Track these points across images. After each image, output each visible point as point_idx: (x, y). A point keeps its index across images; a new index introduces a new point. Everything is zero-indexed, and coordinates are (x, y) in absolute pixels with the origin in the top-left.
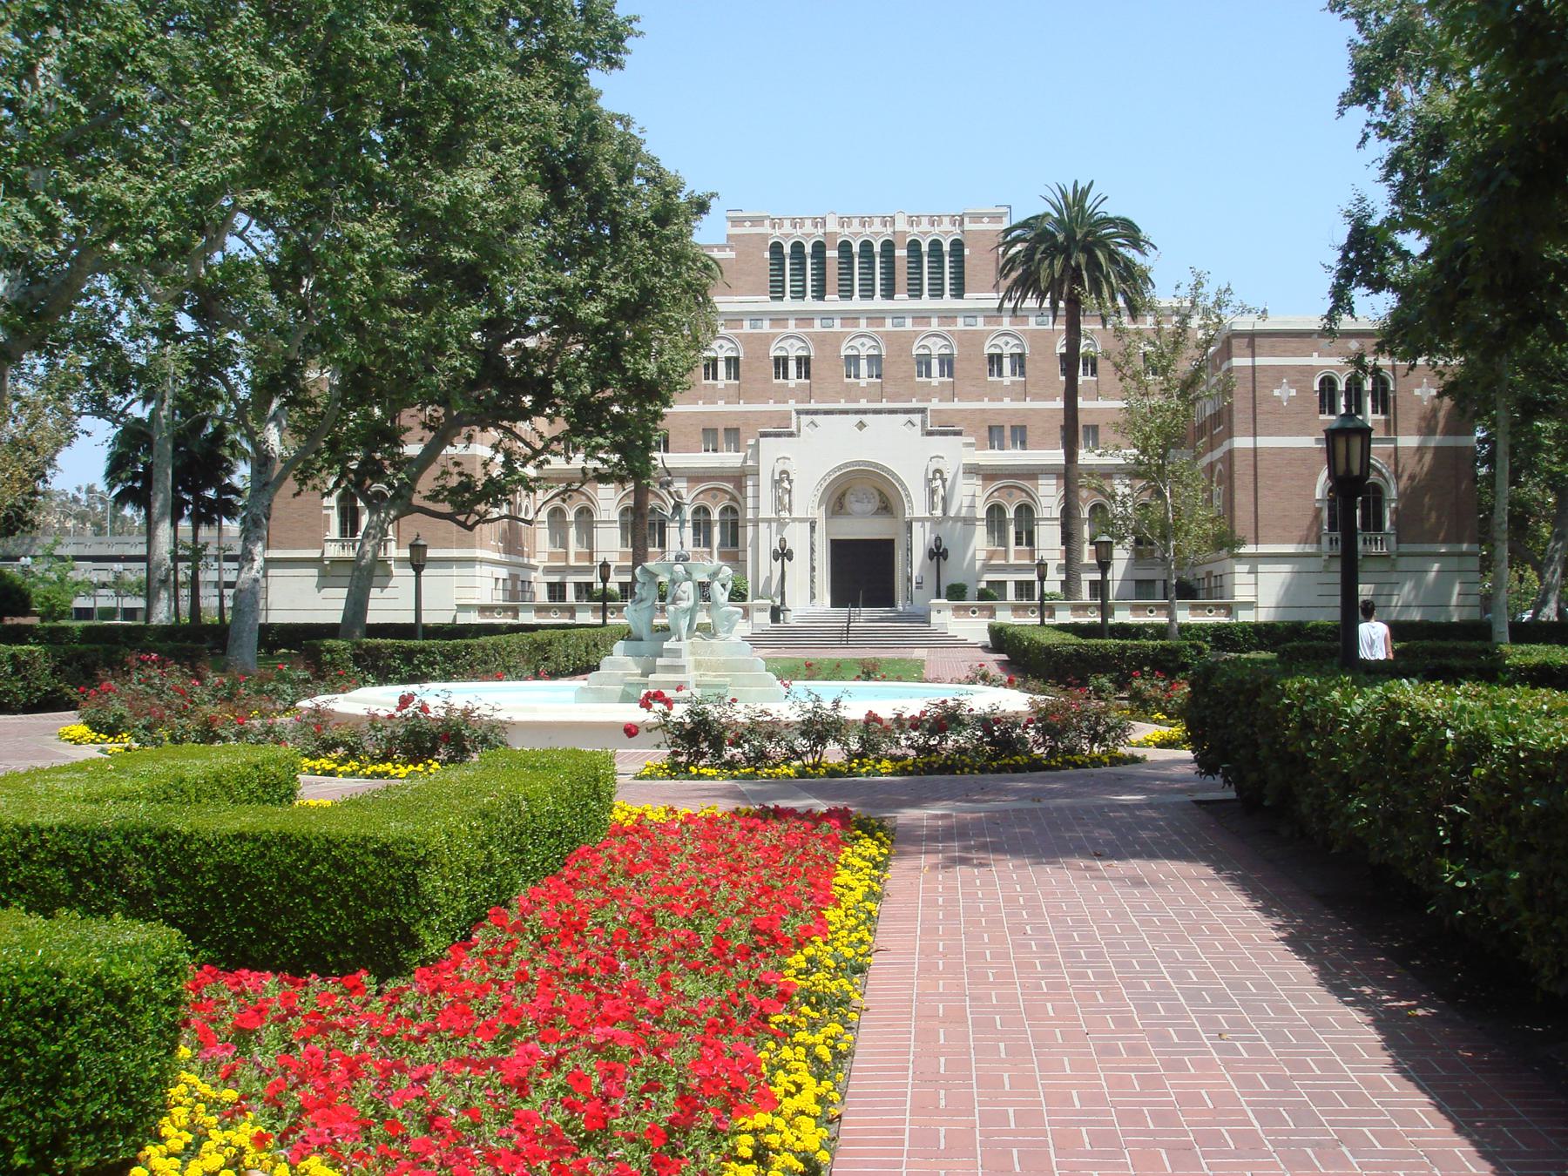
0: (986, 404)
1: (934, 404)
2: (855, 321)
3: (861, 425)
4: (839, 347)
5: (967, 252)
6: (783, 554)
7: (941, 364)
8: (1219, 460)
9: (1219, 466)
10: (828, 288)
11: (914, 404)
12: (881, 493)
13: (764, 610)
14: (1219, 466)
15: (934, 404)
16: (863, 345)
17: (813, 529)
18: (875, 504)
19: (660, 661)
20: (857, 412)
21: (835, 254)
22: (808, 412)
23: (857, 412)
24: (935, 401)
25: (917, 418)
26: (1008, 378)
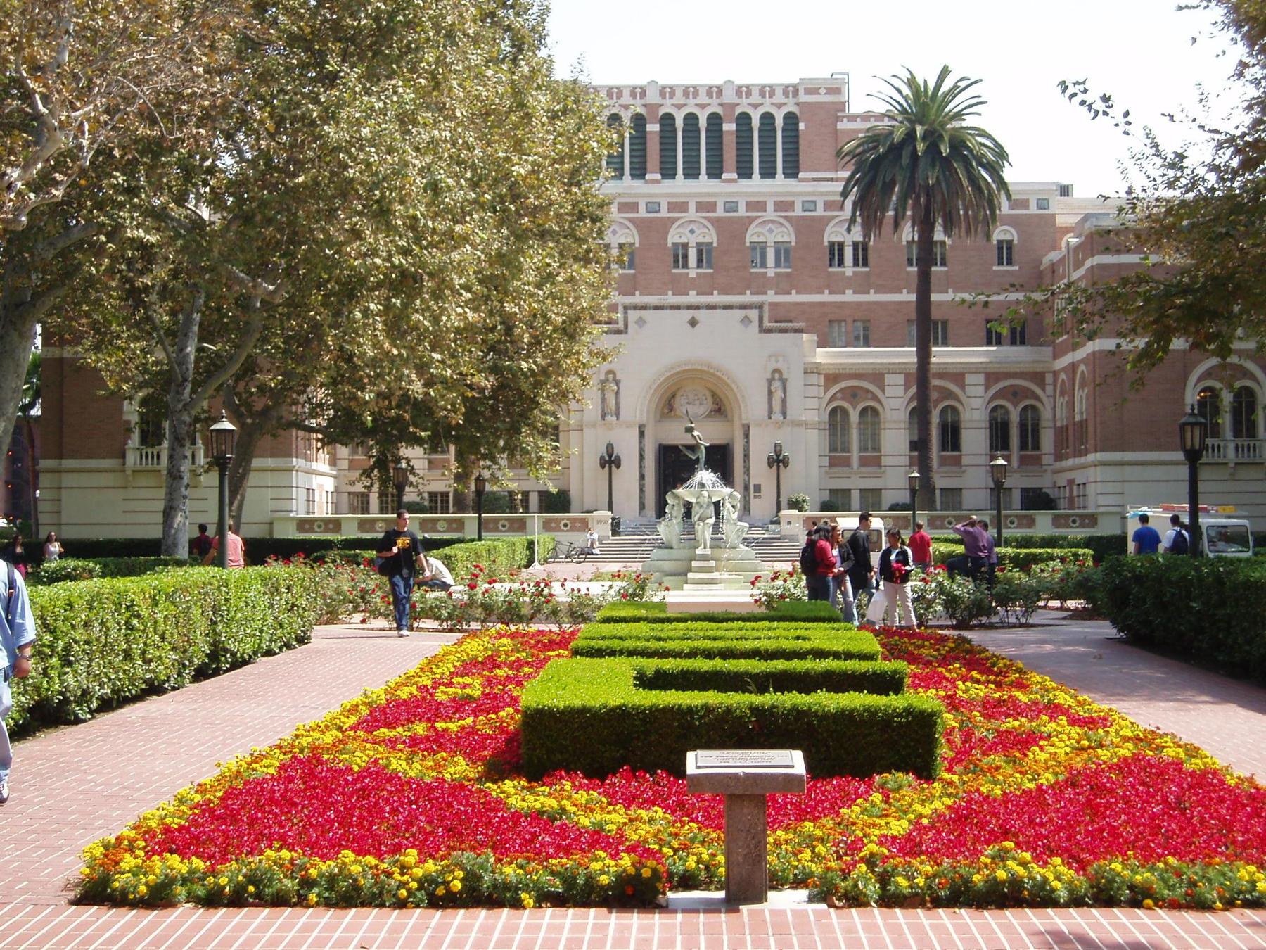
0: (826, 297)
1: (771, 297)
2: (691, 202)
3: (693, 323)
4: (823, 231)
5: (802, 126)
6: (610, 461)
7: (777, 253)
8: (1081, 361)
9: (1082, 367)
10: (649, 165)
11: (748, 298)
12: (714, 395)
13: (606, 522)
14: (1082, 367)
15: (771, 297)
16: (771, 231)
17: (642, 434)
18: (708, 405)
19: (694, 564)
20: (689, 307)
21: (733, 127)
22: (635, 308)
23: (689, 307)
24: (771, 292)
25: (754, 314)
26: (849, 269)
